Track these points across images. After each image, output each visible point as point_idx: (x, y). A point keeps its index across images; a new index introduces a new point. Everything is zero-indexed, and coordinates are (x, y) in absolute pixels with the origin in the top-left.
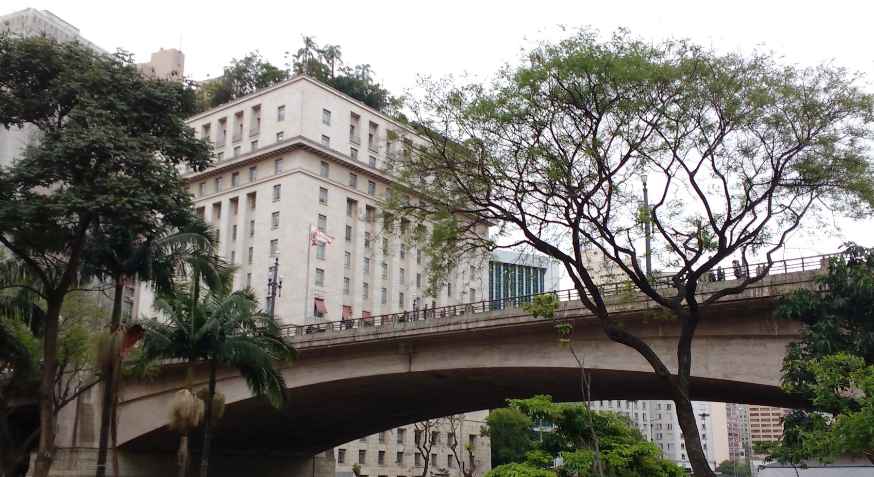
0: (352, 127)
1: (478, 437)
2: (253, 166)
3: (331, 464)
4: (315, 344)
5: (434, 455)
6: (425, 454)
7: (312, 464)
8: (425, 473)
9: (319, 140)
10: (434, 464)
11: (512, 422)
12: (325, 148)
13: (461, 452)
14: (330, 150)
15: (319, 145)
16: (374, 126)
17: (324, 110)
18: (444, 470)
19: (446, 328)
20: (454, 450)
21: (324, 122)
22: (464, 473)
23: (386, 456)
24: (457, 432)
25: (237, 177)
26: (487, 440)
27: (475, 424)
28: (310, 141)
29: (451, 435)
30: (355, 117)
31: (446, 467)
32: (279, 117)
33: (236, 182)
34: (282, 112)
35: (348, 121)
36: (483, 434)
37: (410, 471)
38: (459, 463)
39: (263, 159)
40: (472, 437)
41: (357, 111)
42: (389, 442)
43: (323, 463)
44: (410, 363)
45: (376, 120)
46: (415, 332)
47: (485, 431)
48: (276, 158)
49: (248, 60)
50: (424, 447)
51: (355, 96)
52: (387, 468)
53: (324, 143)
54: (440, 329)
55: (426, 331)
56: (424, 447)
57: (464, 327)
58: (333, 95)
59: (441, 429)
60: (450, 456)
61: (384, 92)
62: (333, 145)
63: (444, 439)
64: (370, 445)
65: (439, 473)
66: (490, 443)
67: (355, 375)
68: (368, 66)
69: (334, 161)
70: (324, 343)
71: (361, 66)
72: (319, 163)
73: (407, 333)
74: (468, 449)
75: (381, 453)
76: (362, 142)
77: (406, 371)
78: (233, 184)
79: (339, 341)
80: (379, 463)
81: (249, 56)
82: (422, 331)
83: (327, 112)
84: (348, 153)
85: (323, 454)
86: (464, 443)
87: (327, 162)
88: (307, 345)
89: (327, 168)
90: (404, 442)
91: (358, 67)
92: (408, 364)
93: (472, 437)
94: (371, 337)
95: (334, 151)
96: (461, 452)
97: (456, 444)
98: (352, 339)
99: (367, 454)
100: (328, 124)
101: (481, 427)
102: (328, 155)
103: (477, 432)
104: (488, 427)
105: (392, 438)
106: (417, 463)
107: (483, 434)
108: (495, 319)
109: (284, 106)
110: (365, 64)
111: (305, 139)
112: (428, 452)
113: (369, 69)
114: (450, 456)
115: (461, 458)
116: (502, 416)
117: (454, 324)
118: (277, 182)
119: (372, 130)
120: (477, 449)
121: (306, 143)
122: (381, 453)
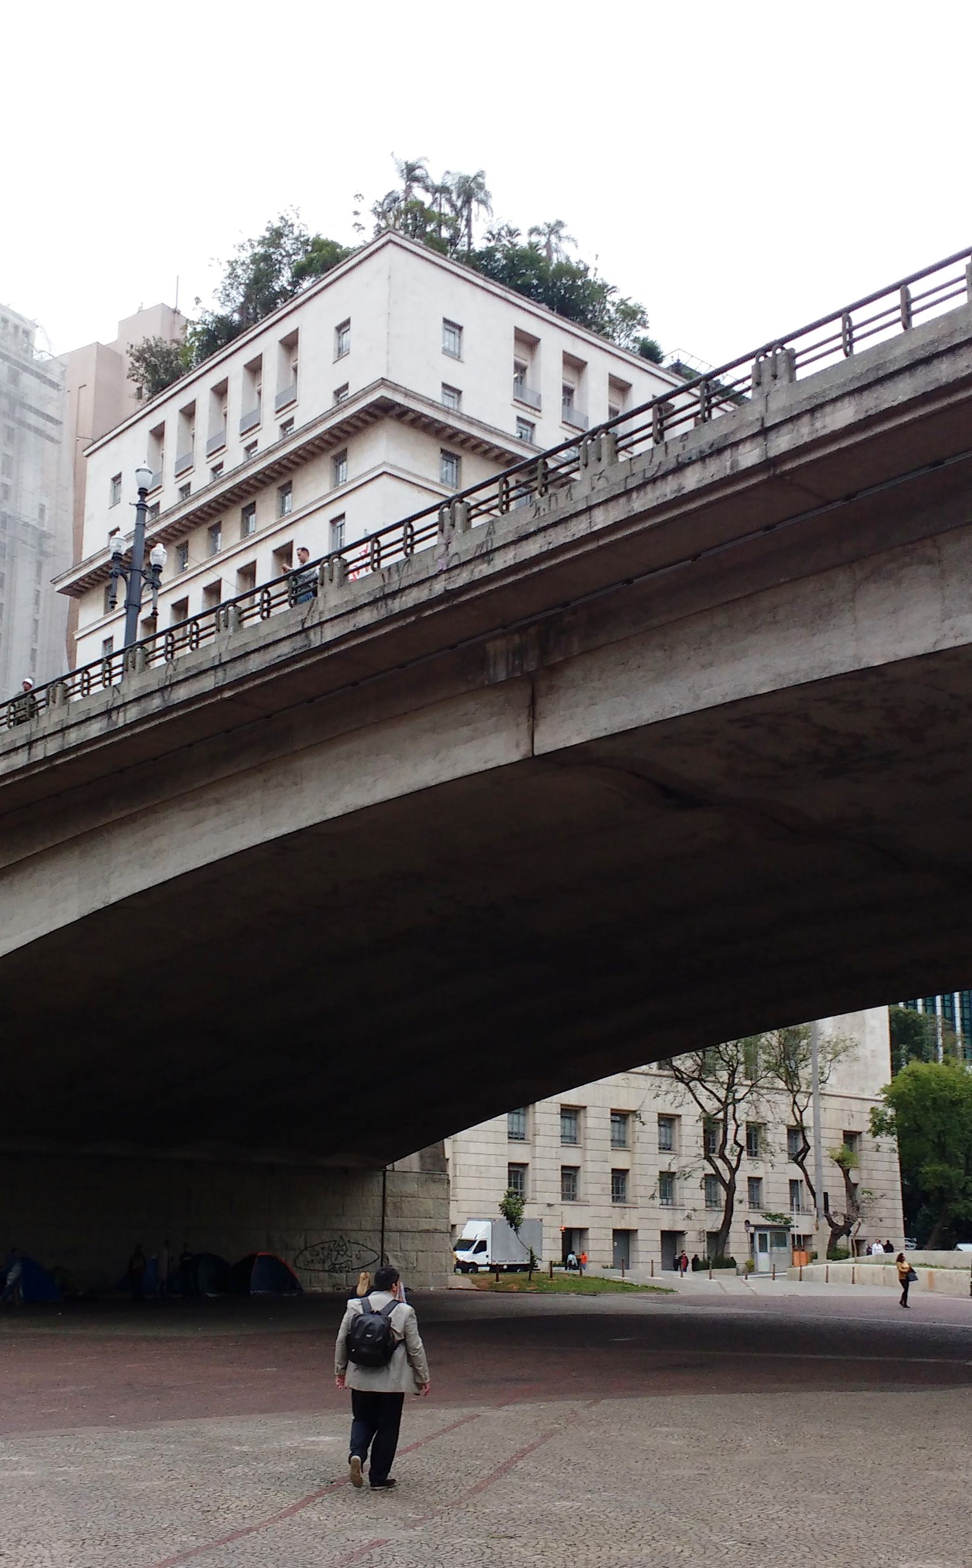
0: (520, 369)
1: (867, 1137)
2: (283, 482)
3: (436, 1189)
4: (182, 693)
5: (754, 1182)
6: (727, 1176)
7: (378, 1191)
8: (727, 1223)
9: (437, 395)
10: (755, 1202)
11: (955, 1096)
12: (447, 411)
13: (818, 1166)
14: (461, 417)
15: (432, 404)
16: (575, 365)
17: (446, 321)
18: (780, 1216)
19: (667, 490)
20: (801, 1165)
21: (445, 351)
22: (831, 1224)
23: (631, 1180)
24: (808, 1120)
25: (252, 518)
26: (889, 1142)
27: (856, 1105)
28: (407, 394)
29: (796, 1131)
30: (527, 342)
31: (785, 1210)
32: (340, 350)
33: (252, 527)
34: (346, 337)
35: (508, 352)
36: (878, 1128)
37: (689, 1217)
38: (814, 1194)
39: (305, 459)
40: (850, 1137)
41: (532, 326)
42: (638, 1147)
43: (412, 1187)
44: (533, 716)
45: (580, 351)
46: (532, 548)
47: (882, 1120)
48: (334, 452)
49: (276, 236)
50: (723, 1157)
51: (525, 290)
52: (633, 1211)
53: (449, 402)
54: (640, 503)
55: (580, 528)
56: (723, 1157)
57: (749, 456)
58: (468, 285)
59: (767, 1113)
60: (794, 1183)
61: (603, 290)
62: (469, 407)
63: (777, 1137)
64: (589, 1155)
65: (769, 1223)
66: (895, 1146)
67: (334, 810)
68: (560, 224)
69: (474, 447)
70: (208, 683)
71: (542, 227)
72: (438, 455)
73: (502, 561)
74: (840, 1162)
75: (619, 1176)
76: (545, 405)
77: (515, 756)
78: (245, 531)
79: (255, 663)
80: (614, 1199)
81: (277, 224)
82: (560, 537)
83: (453, 327)
84: (512, 429)
85: (412, 1162)
86: (825, 1143)
87: (457, 452)
88: (156, 703)
89: (458, 467)
90: (676, 1146)
91: (534, 231)
92: (523, 718)
93: (850, 1137)
94: (366, 618)
95: (471, 421)
96: (818, 1166)
97: (807, 1148)
98: (299, 642)
99: (582, 1177)
100: (458, 358)
101: (873, 1110)
102: (457, 432)
103: (862, 1124)
104: (891, 1112)
105: (644, 1138)
106: (711, 1201)
107: (878, 1128)
108: (911, 368)
109: (348, 322)
110: (552, 222)
111: (395, 387)
112: (733, 1171)
113: (563, 232)
114: (794, 1183)
115: (819, 1181)
116: (928, 1081)
117: (703, 458)
118: (334, 511)
119: (571, 378)
120: (863, 1164)
121: (399, 399)
122: (619, 1176)
